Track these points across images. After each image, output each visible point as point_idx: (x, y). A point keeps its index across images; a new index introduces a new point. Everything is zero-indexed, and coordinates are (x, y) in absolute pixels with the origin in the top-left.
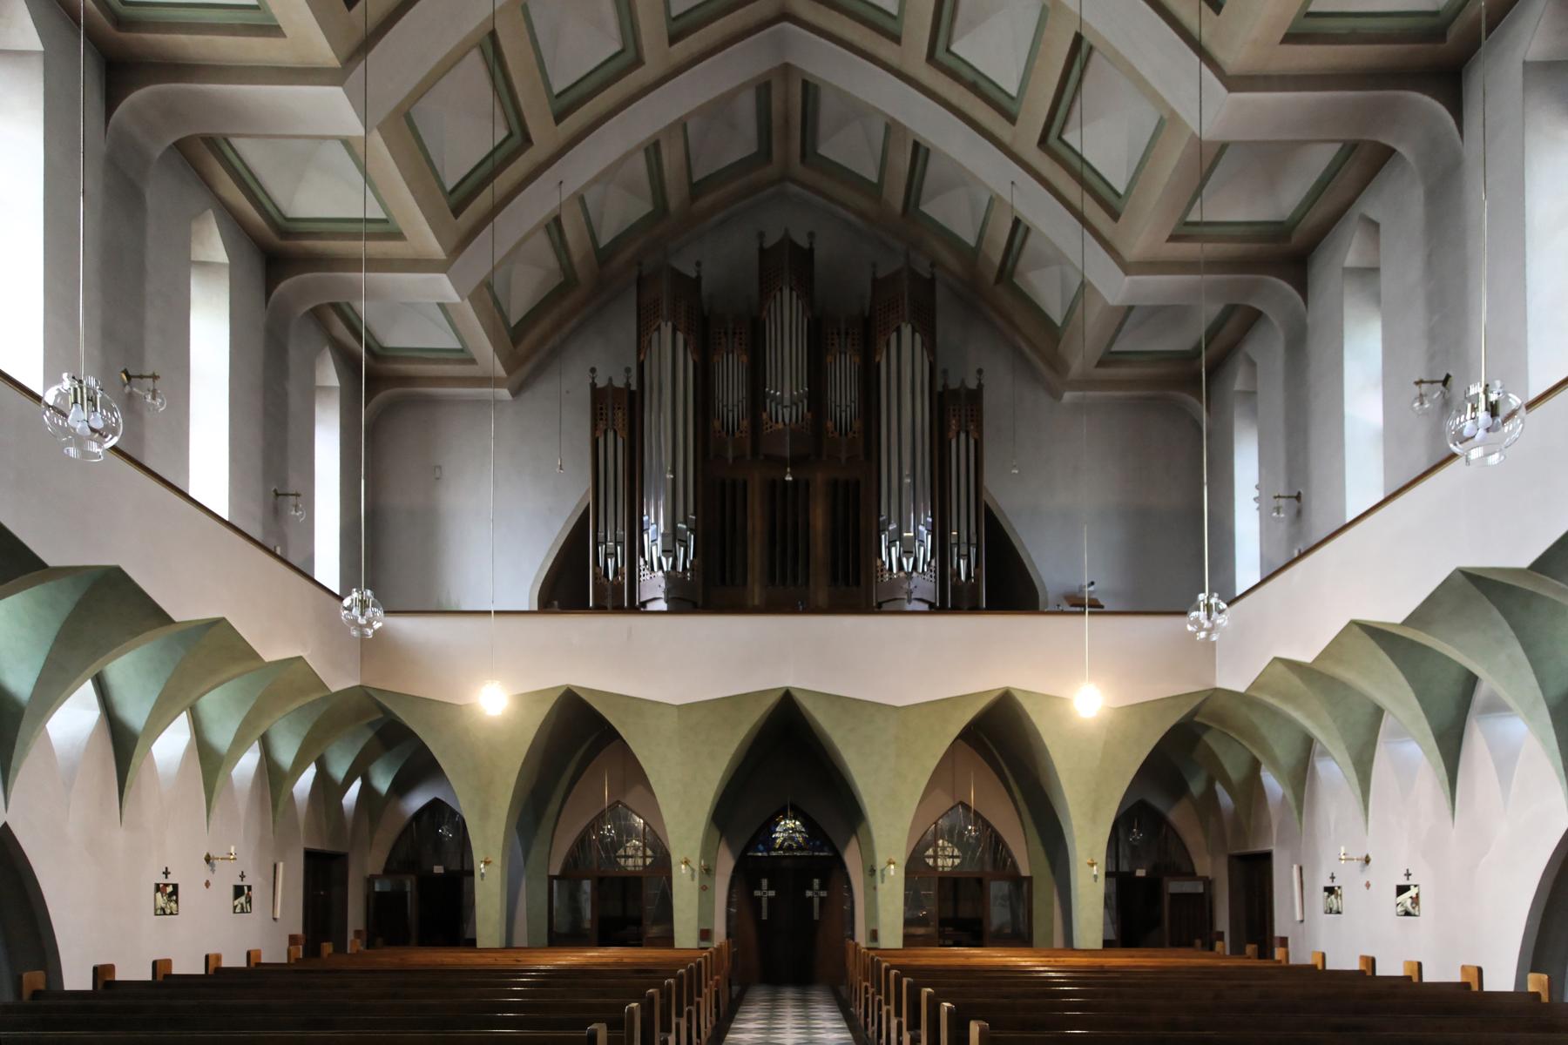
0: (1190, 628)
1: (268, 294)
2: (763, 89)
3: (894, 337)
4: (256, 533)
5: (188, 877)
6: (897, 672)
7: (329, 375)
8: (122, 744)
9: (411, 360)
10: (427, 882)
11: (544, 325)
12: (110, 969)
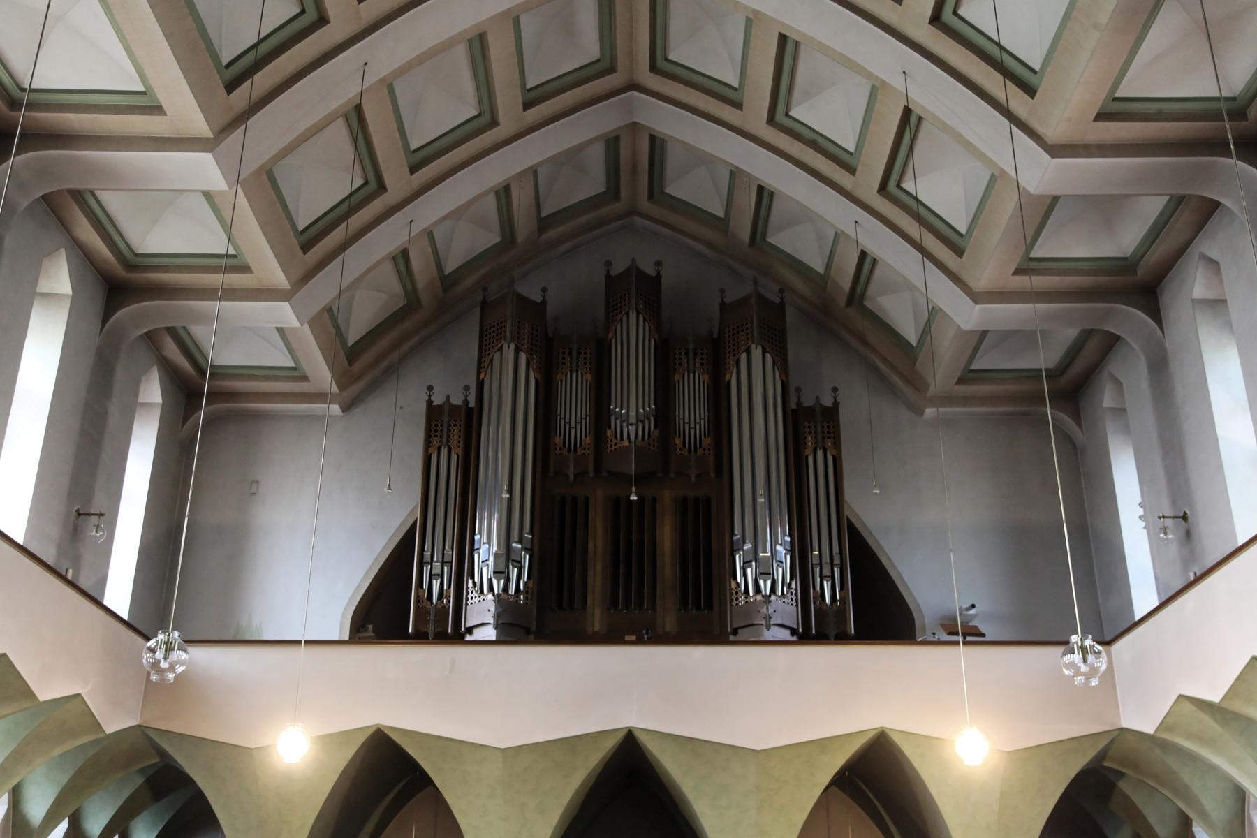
0: (1066, 672)
1: (105, 320)
2: (612, 143)
3: (744, 357)
4: (49, 556)
7: (153, 392)
11: (385, 342)
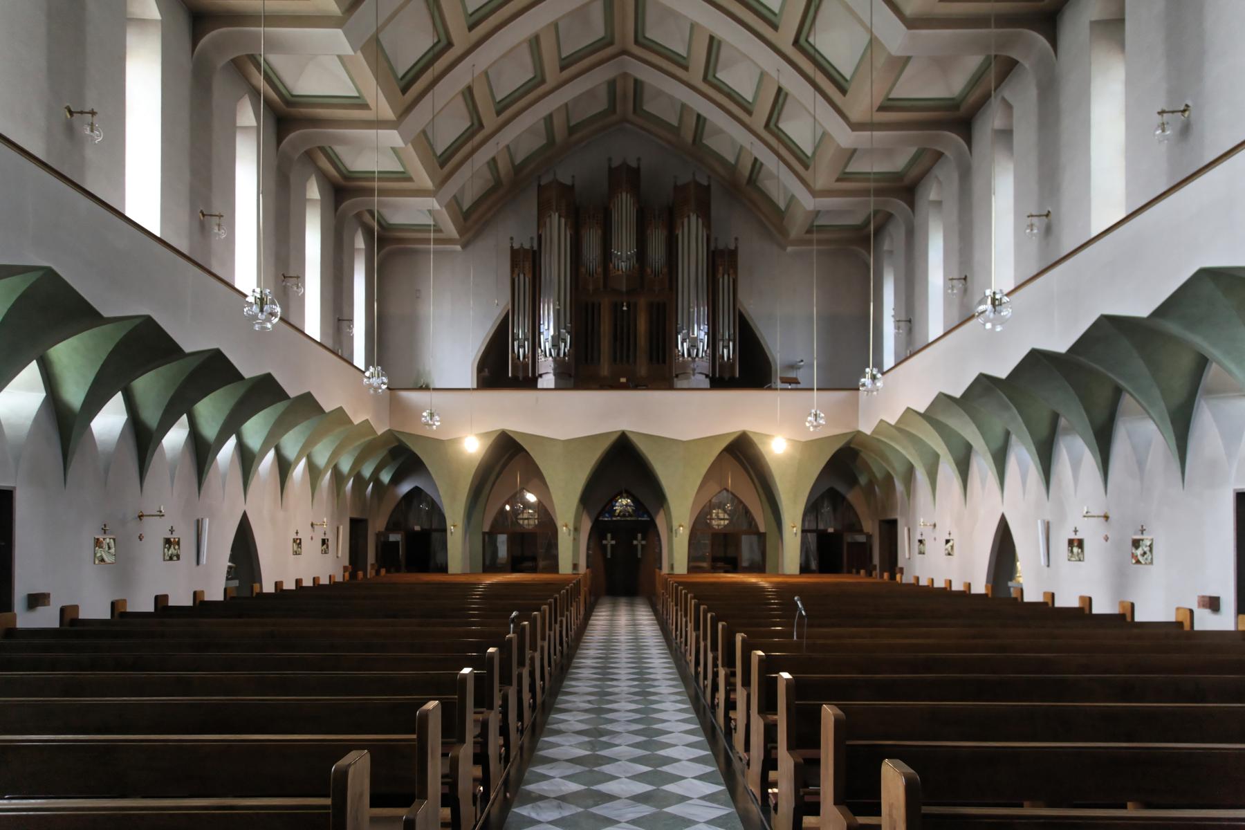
1: (194, 44)
2: (612, 84)
5: (305, 536)
6: (684, 421)
8: (284, 467)
9: (367, 179)
10: (411, 537)
12: (165, 597)
